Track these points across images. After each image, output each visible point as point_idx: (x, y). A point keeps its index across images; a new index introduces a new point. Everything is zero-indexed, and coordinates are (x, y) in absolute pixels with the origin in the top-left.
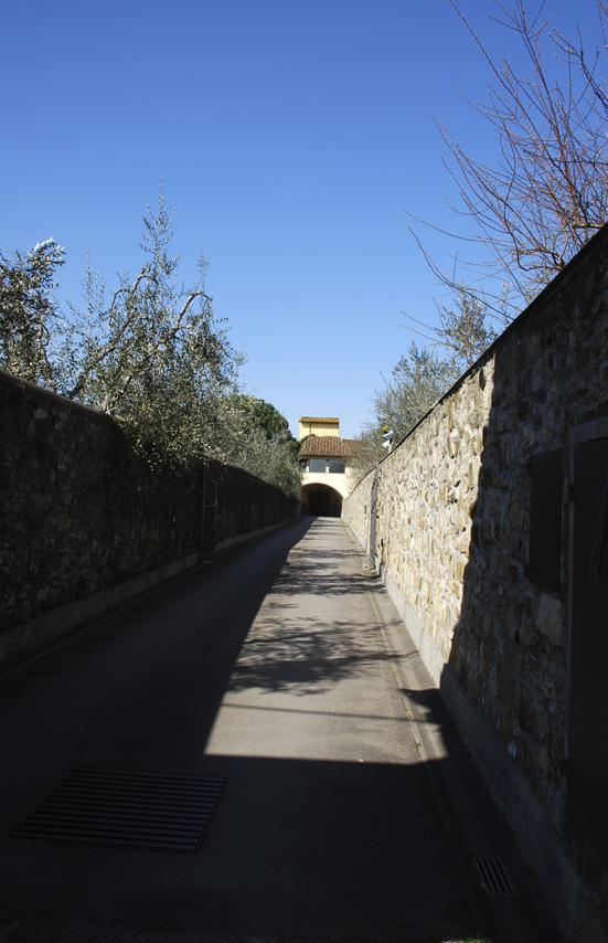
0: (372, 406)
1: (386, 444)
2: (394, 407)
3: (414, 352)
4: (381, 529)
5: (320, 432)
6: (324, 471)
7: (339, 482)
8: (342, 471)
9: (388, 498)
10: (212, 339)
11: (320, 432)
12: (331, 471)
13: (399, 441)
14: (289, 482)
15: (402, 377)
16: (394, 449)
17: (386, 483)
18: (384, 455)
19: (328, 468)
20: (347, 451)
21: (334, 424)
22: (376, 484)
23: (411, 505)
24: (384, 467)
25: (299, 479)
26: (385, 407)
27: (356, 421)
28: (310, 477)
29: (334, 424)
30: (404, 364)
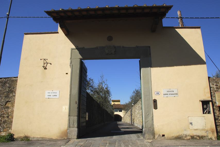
0: (129, 98)
1: (133, 104)
2: (133, 98)
3: (136, 90)
4: (133, 117)
5: (116, 103)
6: (118, 112)
7: (121, 114)
8: (121, 111)
9: (134, 112)
10: (108, 91)
11: (116, 103)
12: (119, 111)
13: (135, 104)
14: (112, 113)
15: (134, 94)
16: (134, 105)
17: (133, 111)
18: (132, 106)
19: (118, 111)
20: (122, 107)
21: (119, 101)
22: (131, 111)
23: (137, 111)
24: (133, 108)
25: (114, 113)
26: (131, 98)
27: (125, 100)
28: (116, 113)
29: (119, 101)
30: (134, 92)
